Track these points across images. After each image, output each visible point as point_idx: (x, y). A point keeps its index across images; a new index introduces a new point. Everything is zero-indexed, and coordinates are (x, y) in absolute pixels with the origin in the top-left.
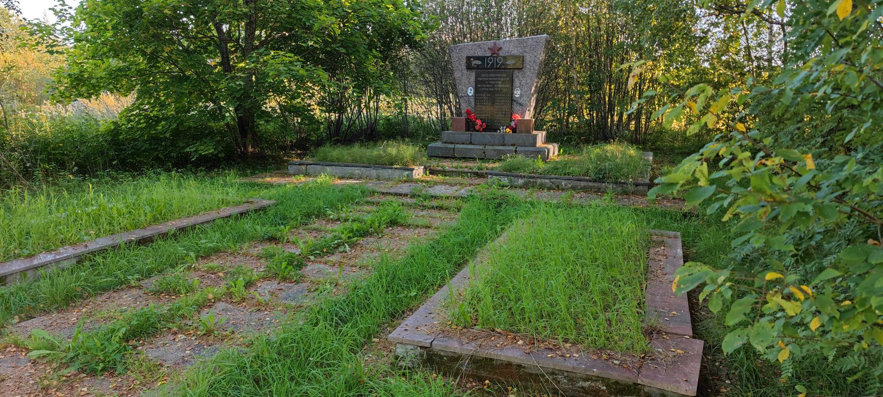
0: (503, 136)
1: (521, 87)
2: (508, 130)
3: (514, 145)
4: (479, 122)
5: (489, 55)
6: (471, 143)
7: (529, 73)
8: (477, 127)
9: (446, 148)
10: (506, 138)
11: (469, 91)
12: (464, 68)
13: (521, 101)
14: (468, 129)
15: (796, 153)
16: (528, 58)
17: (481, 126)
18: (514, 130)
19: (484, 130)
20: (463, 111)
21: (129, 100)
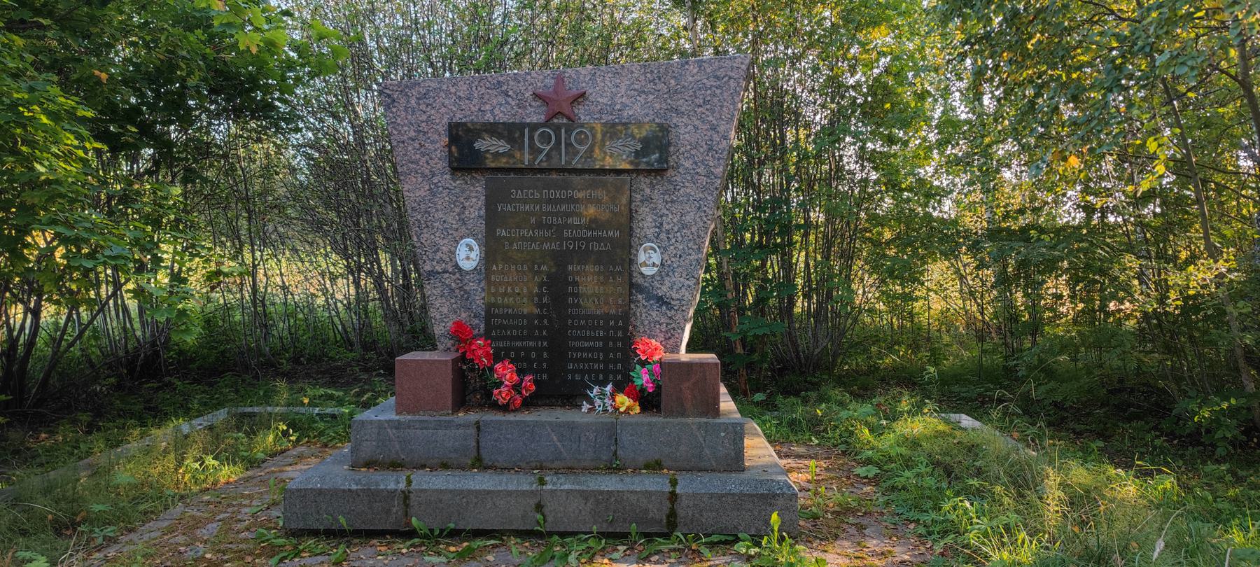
0: (611, 432)
1: (662, 236)
2: (623, 401)
3: (655, 466)
4: (506, 373)
5: (536, 118)
6: (479, 464)
7: (690, 189)
8: (501, 395)
9: (373, 495)
10: (625, 437)
11: (462, 252)
12: (441, 165)
13: (663, 290)
14: (461, 402)
15: (282, 507)
16: (686, 133)
17: (517, 387)
18: (649, 402)
19: (529, 403)
20: (438, 330)
21: (124, 476)
